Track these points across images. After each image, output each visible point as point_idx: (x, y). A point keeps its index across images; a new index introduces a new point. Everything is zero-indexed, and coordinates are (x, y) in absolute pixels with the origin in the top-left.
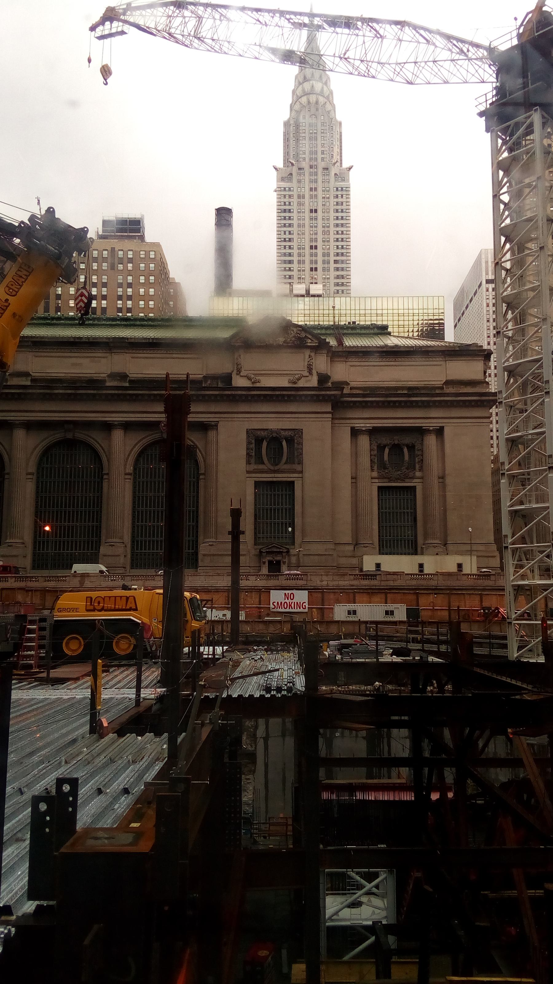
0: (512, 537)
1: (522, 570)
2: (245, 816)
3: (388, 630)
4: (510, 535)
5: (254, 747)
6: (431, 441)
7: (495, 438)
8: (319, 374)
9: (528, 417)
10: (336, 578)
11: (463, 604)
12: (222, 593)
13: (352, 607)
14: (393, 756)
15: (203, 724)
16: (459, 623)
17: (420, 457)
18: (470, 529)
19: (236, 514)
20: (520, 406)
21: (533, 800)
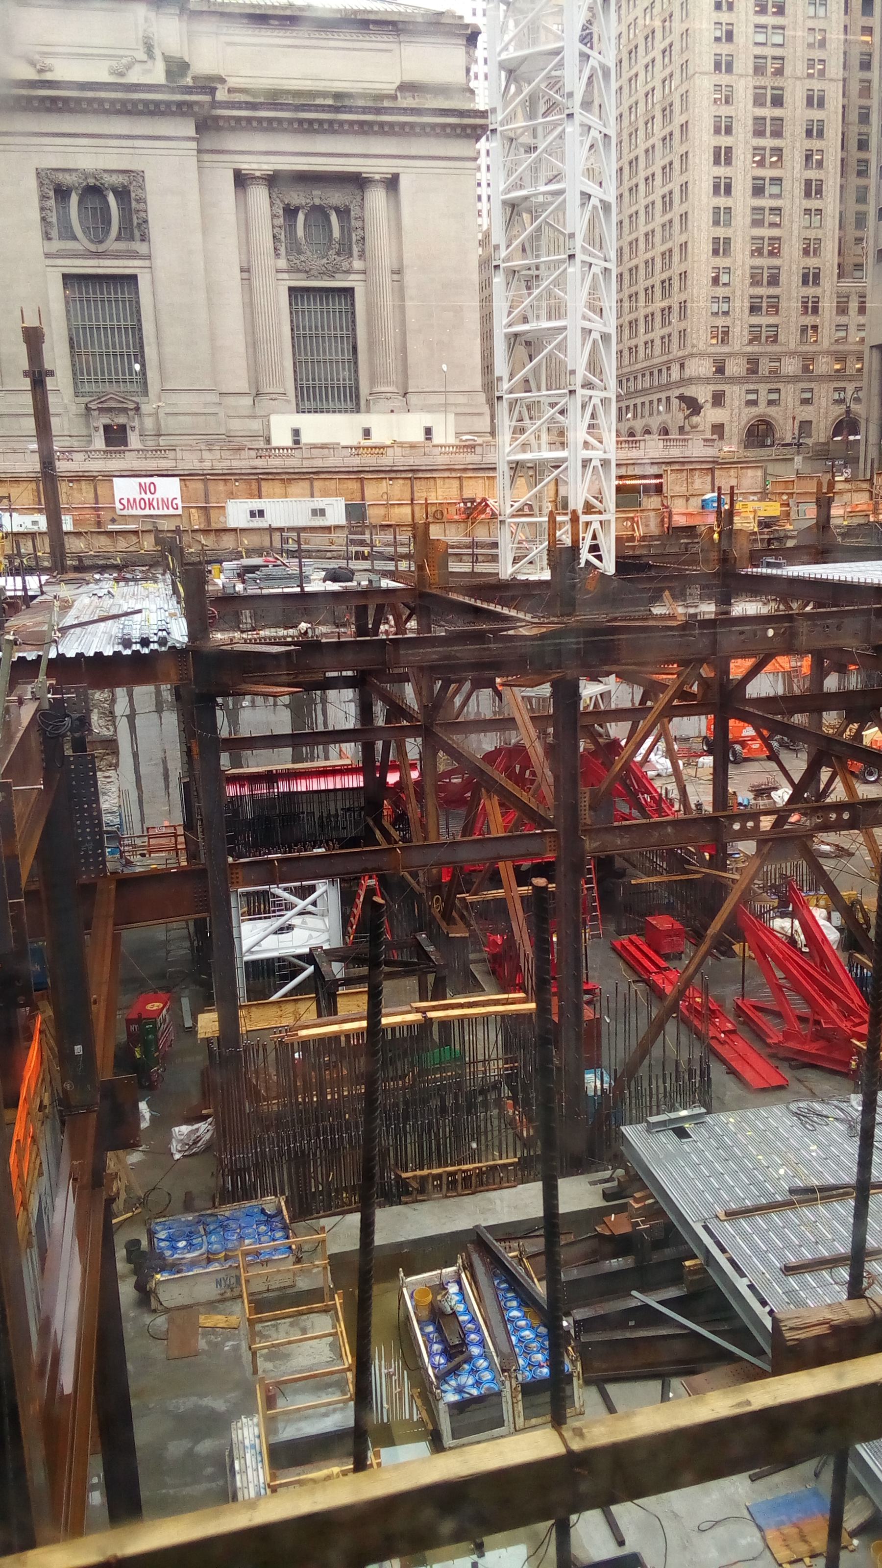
0: (510, 380)
1: (523, 437)
2: (109, 829)
3: (317, 541)
4: (506, 378)
5: (112, 729)
6: (377, 198)
7: (484, 198)
8: (167, 59)
9: (539, 160)
10: (226, 454)
11: (433, 494)
12: (25, 484)
13: (256, 504)
14: (331, 728)
15: (21, 702)
16: (427, 525)
17: (360, 231)
18: (444, 367)
19: (33, 338)
20: (526, 139)
21: (528, 772)
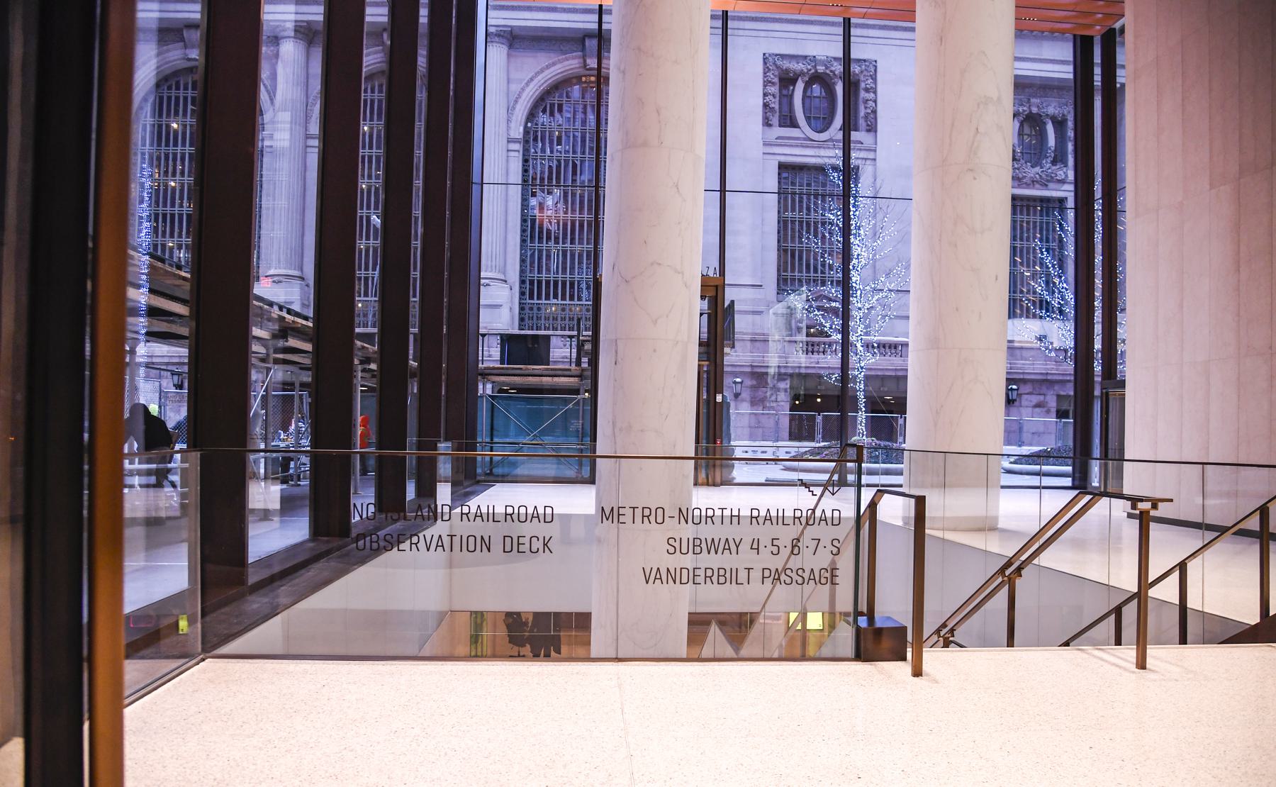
6: (572, 445)
17: (871, 103)
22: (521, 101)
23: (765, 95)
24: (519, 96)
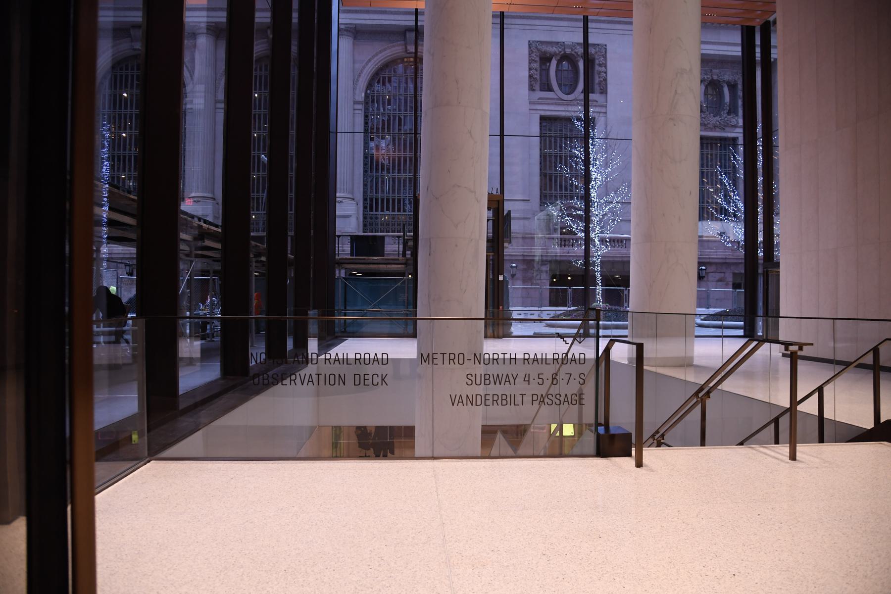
22: (362, 75)
23: (530, 69)
24: (361, 72)
